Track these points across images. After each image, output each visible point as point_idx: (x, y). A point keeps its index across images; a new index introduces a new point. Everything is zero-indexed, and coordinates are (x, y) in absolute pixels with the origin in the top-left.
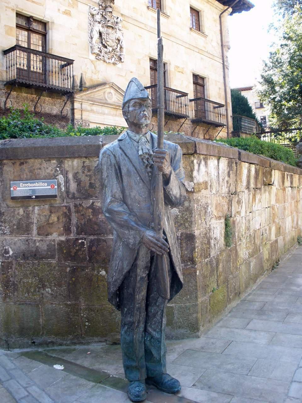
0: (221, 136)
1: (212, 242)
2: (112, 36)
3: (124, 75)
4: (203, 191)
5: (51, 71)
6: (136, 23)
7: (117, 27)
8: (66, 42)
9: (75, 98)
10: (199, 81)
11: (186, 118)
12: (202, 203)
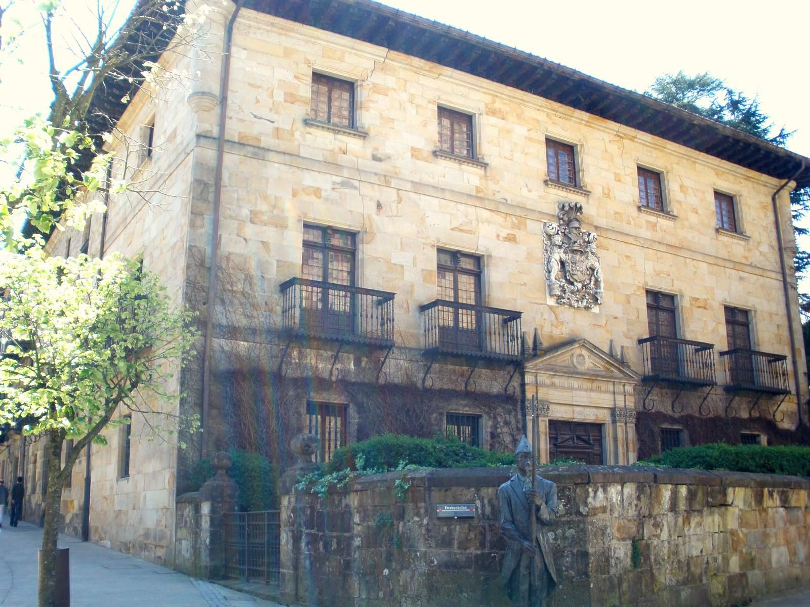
0: (785, 409)
1: (613, 562)
2: (581, 266)
4: (600, 515)
6: (620, 237)
7: (588, 250)
8: (510, 282)
9: (526, 368)
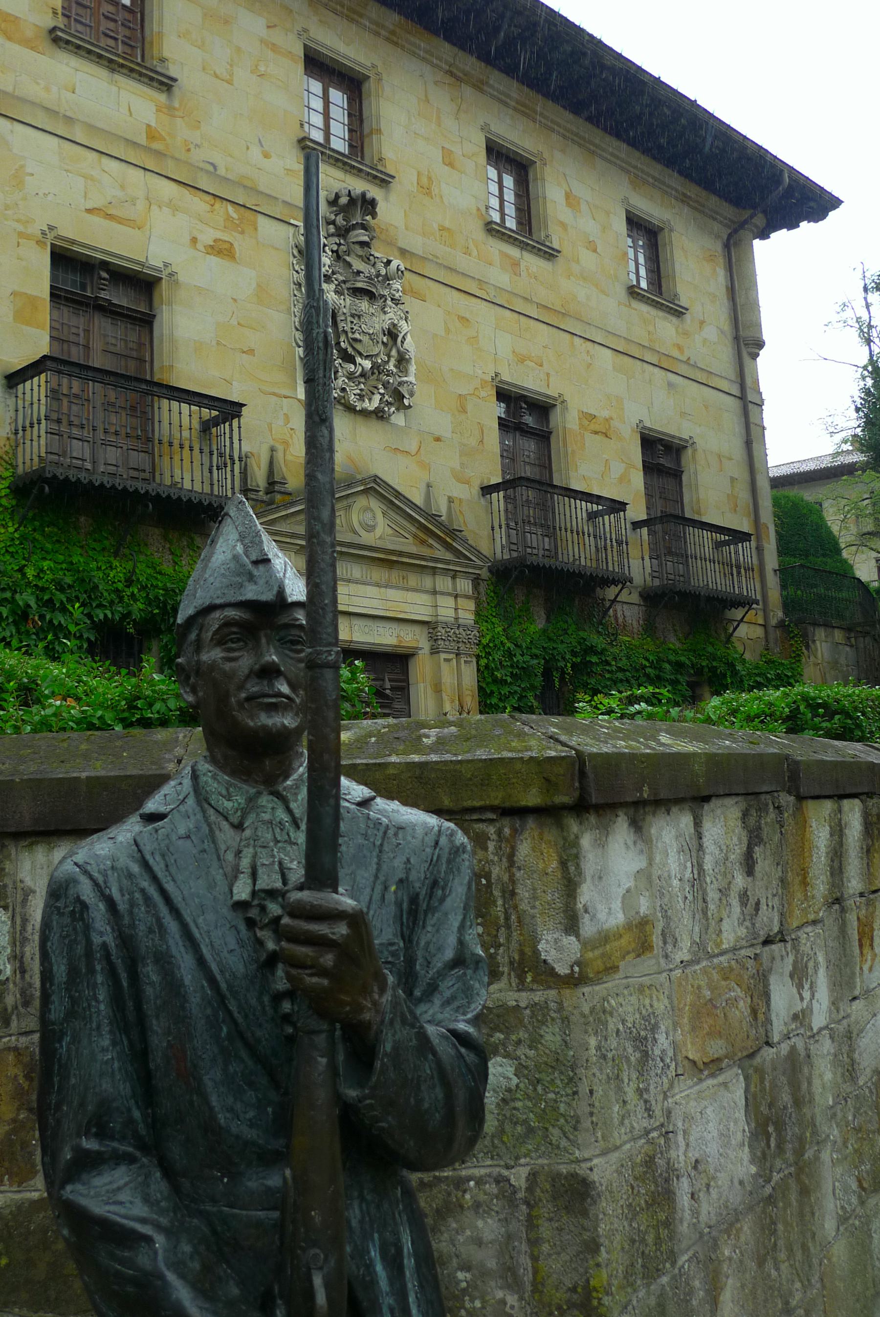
3: (413, 449)
5: (165, 439)
8: (218, 343)
10: (662, 457)
11: (620, 586)
12: (624, 1021)
